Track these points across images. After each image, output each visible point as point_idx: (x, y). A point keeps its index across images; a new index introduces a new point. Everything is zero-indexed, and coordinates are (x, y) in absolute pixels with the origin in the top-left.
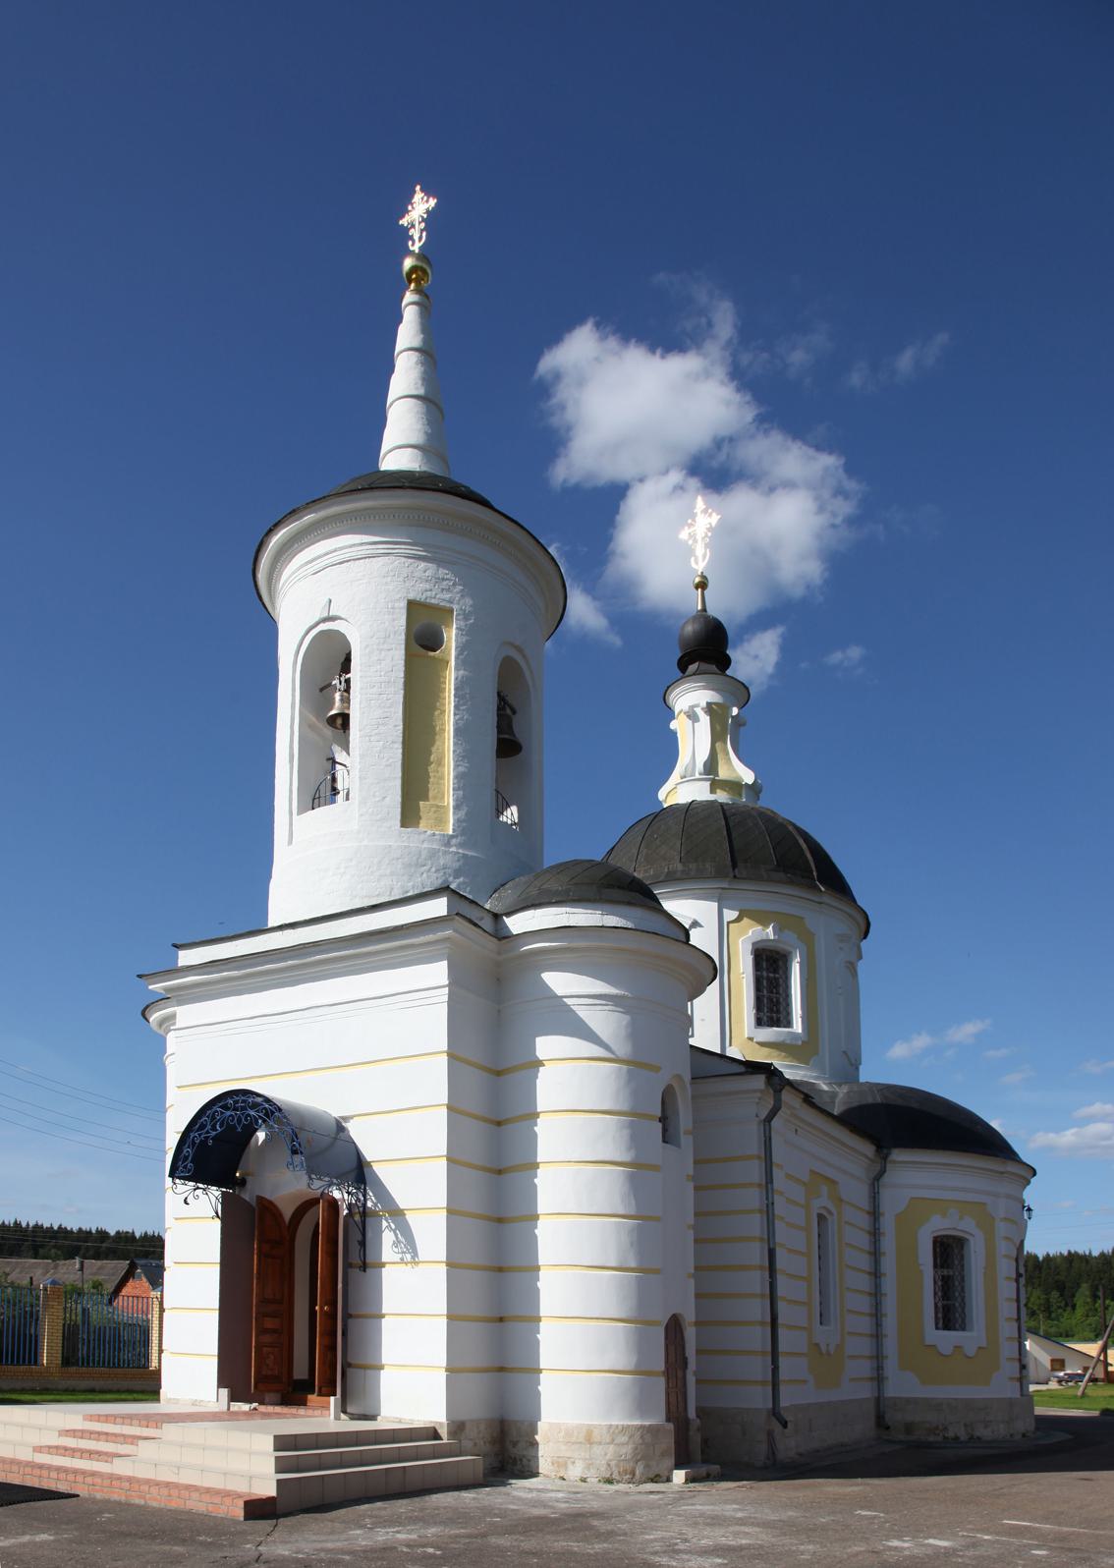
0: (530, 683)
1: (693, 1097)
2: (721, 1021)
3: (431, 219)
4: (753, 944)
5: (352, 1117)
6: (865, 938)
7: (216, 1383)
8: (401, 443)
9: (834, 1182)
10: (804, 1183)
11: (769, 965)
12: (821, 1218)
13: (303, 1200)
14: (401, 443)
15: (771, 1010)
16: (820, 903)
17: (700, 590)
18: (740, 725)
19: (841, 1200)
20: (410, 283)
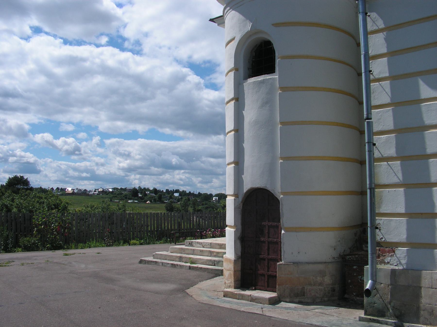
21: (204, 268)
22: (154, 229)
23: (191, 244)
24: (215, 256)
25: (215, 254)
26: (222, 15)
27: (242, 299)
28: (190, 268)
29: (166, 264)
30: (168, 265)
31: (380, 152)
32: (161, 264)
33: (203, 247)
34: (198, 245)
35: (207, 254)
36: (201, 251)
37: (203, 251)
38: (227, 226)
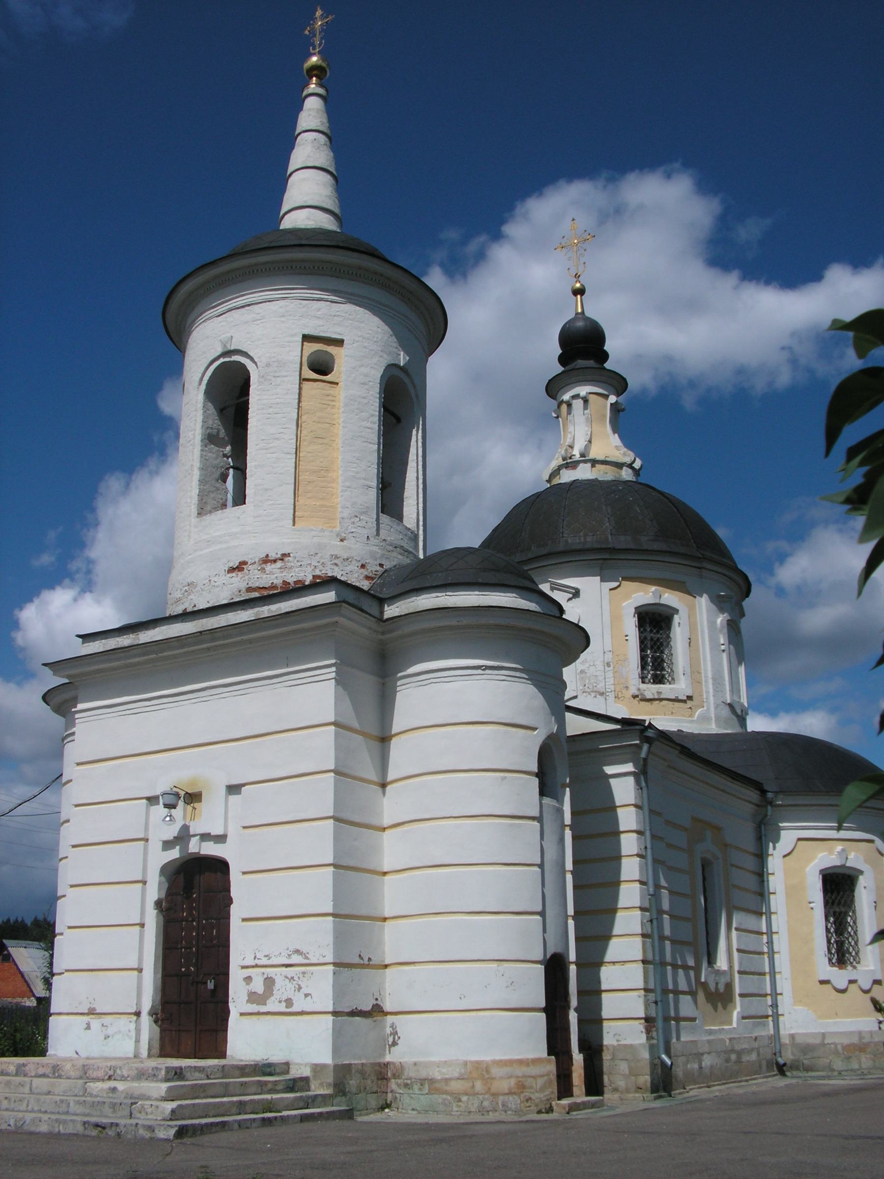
0: (413, 396)
1: (570, 754)
2: (604, 681)
3: (327, 30)
4: (636, 608)
5: (244, 785)
6: (747, 595)
7: (315, 1062)
8: (307, 196)
9: (718, 829)
10: (686, 829)
11: (654, 624)
12: (706, 865)
13: (844, 376)
14: (307, 196)
15: (655, 668)
16: (700, 568)
17: (579, 296)
18: (619, 411)
19: (726, 845)
20: (311, 78)
21: (327, 1113)
22: (731, 967)
23: (181, 1073)
24: (270, 1092)
25: (270, 1086)
26: (800, 842)
27: (584, 1109)
28: (304, 1118)
29: (249, 1124)
30: (254, 1125)
31: (300, 394)
32: (236, 1126)
33: (208, 1078)
34: (197, 1074)
35: (253, 1089)
36: (242, 1084)
37: (246, 1083)
38: (51, 1015)
